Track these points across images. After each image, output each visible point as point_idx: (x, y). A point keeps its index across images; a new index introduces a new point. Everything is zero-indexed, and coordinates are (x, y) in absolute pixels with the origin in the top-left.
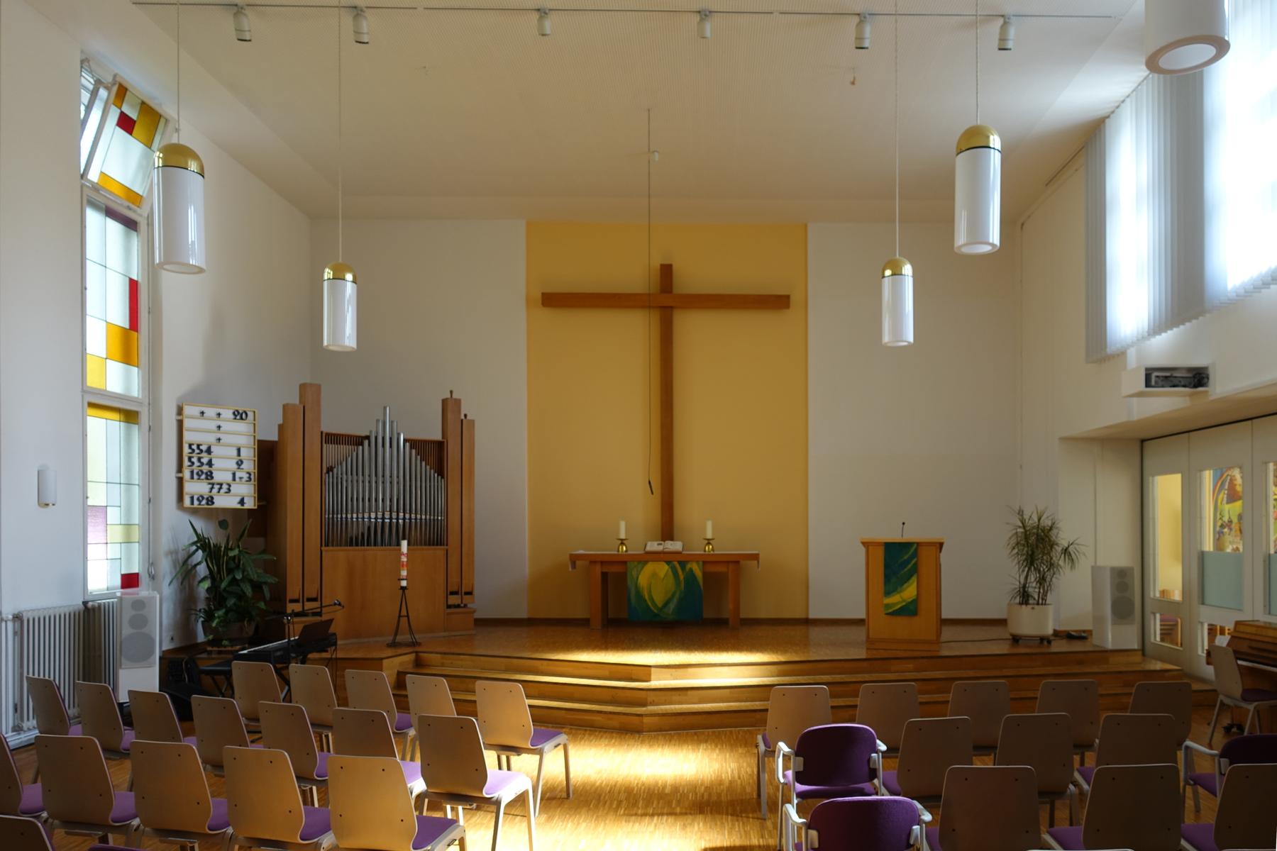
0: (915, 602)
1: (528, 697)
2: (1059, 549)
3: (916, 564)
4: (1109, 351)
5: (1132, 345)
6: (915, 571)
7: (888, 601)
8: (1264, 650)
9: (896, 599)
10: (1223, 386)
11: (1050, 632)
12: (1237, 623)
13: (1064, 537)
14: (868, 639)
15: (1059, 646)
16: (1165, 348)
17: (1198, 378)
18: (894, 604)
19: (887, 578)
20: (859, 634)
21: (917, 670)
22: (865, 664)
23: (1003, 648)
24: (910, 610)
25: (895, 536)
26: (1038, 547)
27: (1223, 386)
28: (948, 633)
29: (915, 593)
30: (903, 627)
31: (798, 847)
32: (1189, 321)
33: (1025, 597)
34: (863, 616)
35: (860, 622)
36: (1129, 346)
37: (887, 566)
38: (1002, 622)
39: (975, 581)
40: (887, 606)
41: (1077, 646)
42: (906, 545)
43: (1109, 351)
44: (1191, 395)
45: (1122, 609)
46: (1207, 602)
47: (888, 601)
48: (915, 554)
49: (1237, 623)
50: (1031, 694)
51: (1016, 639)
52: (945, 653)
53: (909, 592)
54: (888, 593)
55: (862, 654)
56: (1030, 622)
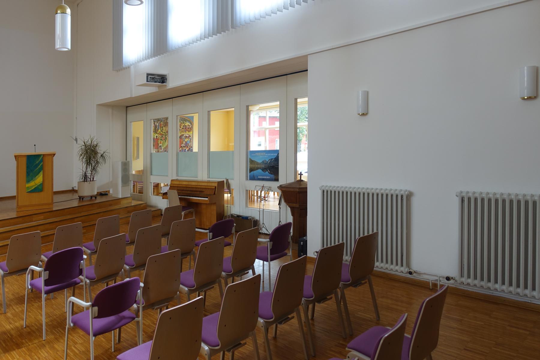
0: (42, 184)
1: (42, 337)
2: (100, 155)
3: (42, 165)
4: (124, 66)
5: (133, 64)
6: (42, 168)
7: (27, 185)
8: (183, 190)
9: (32, 184)
10: (172, 83)
11: (96, 193)
12: (172, 180)
13: (101, 150)
14: (18, 207)
15: (99, 200)
16: (152, 65)
17: (163, 79)
18: (32, 186)
19: (28, 174)
20: (13, 204)
21: (45, 219)
22: (21, 219)
23: (75, 204)
24: (38, 189)
25: (32, 152)
26: (91, 154)
27: (172, 83)
28: (57, 198)
29: (42, 180)
30: (36, 198)
31: (96, 358)
32: (160, 55)
33: (85, 178)
34: (14, 194)
35: (13, 198)
36: (132, 65)
37: (28, 167)
38: (73, 191)
39: (68, 172)
40: (28, 188)
41: (104, 199)
42: (38, 156)
43: (124, 66)
44: (159, 87)
45: (126, 179)
46: (153, 174)
47: (27, 185)
48: (42, 160)
49: (172, 180)
50: (92, 223)
51: (81, 198)
52: (54, 209)
53: (39, 179)
54: (28, 181)
55: (13, 215)
56: (88, 190)
